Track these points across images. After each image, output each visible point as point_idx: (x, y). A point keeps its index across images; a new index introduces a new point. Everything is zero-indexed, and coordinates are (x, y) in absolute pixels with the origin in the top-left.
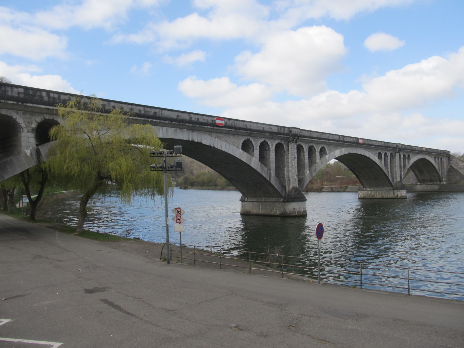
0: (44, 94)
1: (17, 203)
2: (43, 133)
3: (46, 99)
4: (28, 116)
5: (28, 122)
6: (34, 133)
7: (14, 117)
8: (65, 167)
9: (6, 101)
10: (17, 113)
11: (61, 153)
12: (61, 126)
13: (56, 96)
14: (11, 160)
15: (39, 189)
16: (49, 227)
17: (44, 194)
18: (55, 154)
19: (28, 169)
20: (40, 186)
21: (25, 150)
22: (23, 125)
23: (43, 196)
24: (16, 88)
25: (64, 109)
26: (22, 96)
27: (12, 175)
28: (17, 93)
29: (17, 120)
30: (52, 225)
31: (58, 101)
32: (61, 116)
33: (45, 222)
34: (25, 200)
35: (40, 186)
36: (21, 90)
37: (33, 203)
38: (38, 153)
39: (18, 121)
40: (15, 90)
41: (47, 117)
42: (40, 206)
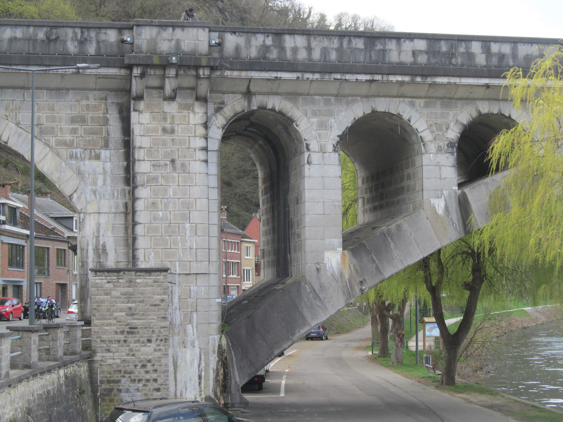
0: (476, 47)
1: (410, 338)
2: (474, 154)
3: (481, 60)
4: (438, 109)
5: (439, 127)
6: (452, 153)
7: (405, 117)
8: (532, 241)
9: (385, 78)
10: (412, 105)
11: (523, 204)
12: (519, 128)
13: (506, 49)
14: (399, 227)
15: (464, 303)
16: (491, 407)
17: (478, 316)
18: (506, 208)
19: (439, 251)
20: (467, 293)
21: (432, 201)
22: (427, 136)
23: (474, 322)
24: (407, 42)
25: (522, 82)
26: (422, 59)
27: (400, 267)
28: (410, 54)
29: (412, 123)
30: (498, 401)
31: (511, 63)
32: (518, 102)
33: (482, 391)
34: (431, 329)
35: (467, 293)
36: (421, 45)
37: (452, 341)
38: (464, 205)
39: (414, 127)
40: (407, 46)
41: (485, 108)
42: (466, 349)
